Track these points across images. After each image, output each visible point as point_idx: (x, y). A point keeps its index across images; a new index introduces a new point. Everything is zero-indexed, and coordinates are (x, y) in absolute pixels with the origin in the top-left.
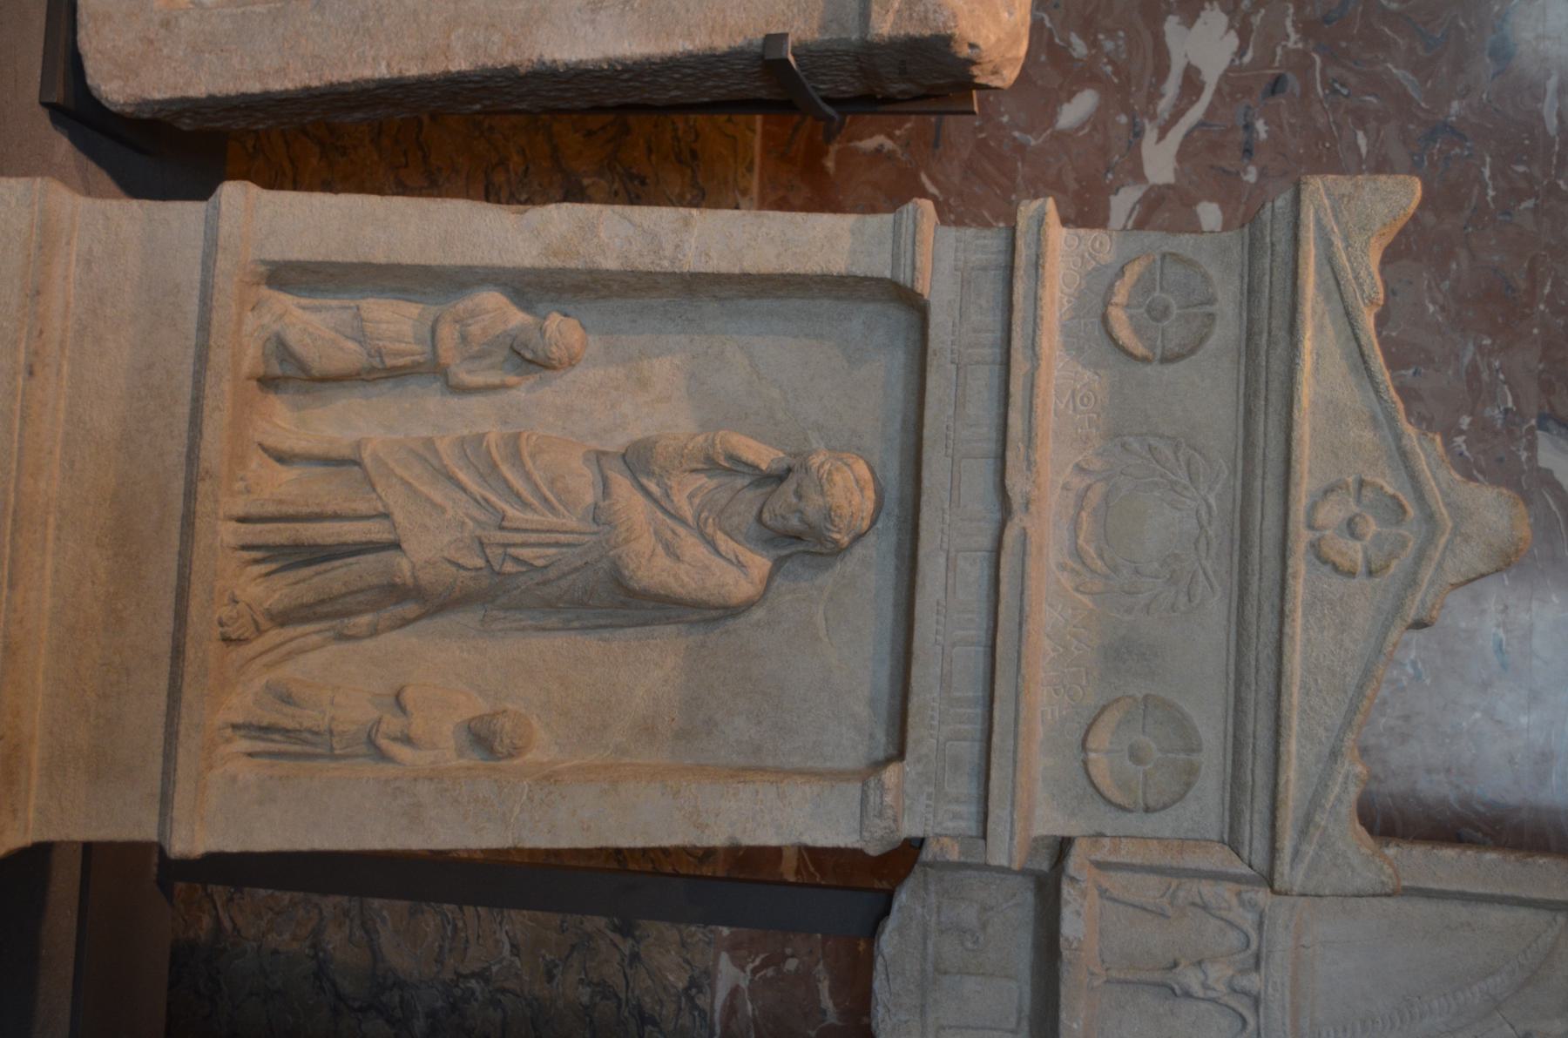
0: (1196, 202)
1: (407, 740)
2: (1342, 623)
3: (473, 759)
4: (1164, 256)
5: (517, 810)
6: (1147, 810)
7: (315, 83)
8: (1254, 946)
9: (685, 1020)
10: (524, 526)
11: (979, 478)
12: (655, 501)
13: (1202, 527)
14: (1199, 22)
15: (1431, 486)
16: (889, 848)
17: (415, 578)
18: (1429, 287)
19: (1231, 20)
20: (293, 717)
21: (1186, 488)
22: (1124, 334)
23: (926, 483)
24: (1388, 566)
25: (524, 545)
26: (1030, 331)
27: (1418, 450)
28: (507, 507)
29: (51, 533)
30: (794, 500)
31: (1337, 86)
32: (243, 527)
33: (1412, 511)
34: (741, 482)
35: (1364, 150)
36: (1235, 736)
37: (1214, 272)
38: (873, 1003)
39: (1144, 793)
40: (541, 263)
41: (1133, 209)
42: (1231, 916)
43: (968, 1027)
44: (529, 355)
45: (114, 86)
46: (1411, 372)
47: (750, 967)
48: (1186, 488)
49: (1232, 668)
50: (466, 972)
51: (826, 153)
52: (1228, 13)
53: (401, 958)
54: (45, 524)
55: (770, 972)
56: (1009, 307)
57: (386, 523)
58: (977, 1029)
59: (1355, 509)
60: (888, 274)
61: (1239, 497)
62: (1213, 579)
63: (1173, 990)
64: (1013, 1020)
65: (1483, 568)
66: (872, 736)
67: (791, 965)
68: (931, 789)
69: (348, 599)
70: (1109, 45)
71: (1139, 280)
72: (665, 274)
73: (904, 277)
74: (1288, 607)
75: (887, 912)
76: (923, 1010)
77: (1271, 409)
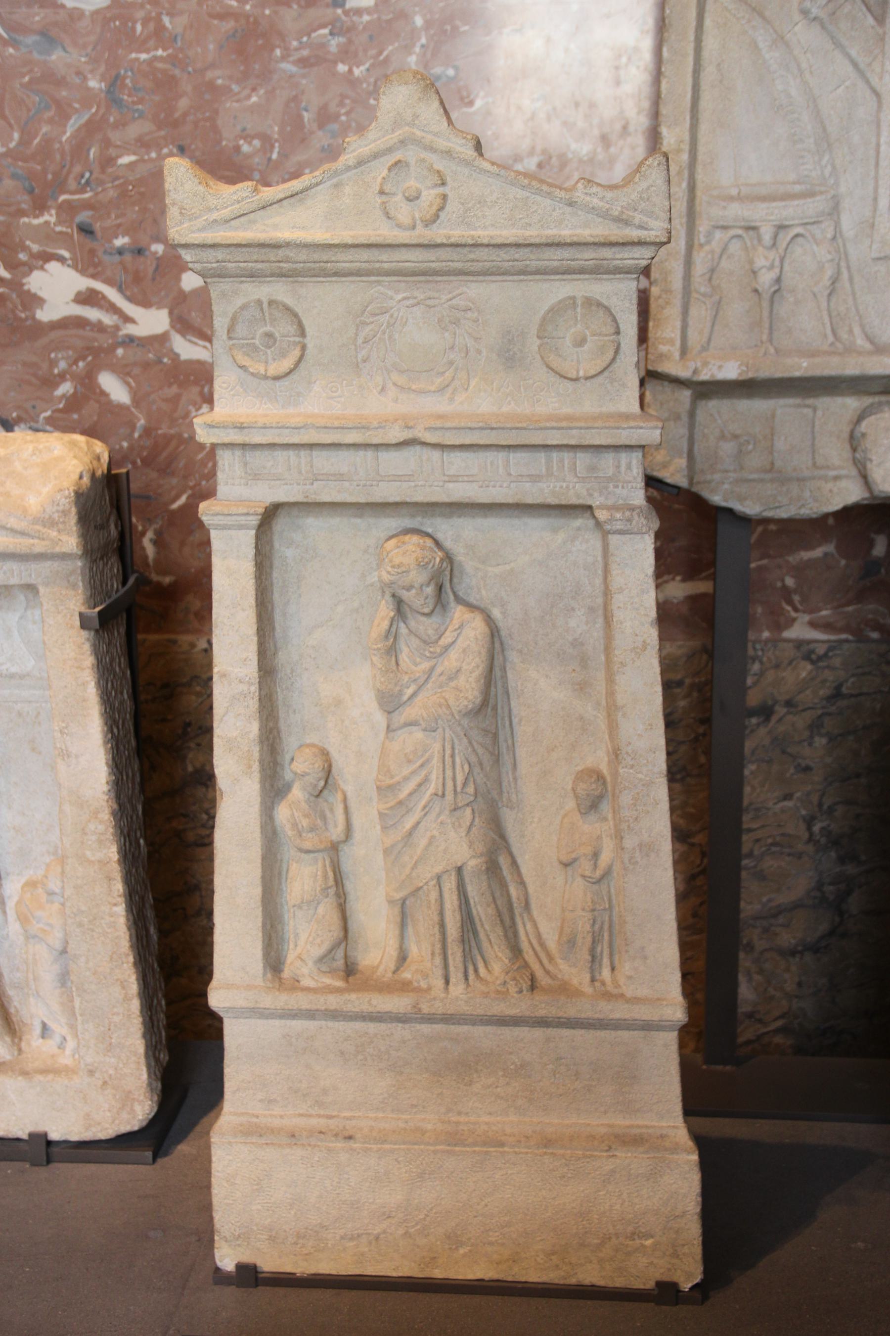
0: (181, 292)
1: (596, 855)
2: (480, 202)
3: (605, 807)
4: (230, 338)
5: (640, 776)
6: (618, 333)
7: (131, 959)
8: (740, 232)
9: (837, 662)
10: (441, 780)
11: (391, 460)
12: (420, 688)
13: (418, 304)
14: (40, 294)
15: (380, 145)
16: (654, 513)
17: (481, 855)
18: (238, 101)
19: (37, 268)
20: (584, 938)
21: (392, 316)
22: (287, 364)
23: (398, 499)
24: (438, 172)
25: (454, 779)
26: (287, 431)
27: (355, 154)
28: (429, 793)
29: (462, 1119)
30: (414, 591)
31: (83, 181)
32: (453, 980)
33: (398, 156)
34: (403, 630)
35: (133, 158)
36: (563, 273)
37: (239, 302)
38: (798, 517)
39: (606, 335)
40: (256, 776)
41: (190, 341)
42: (718, 251)
43: (813, 445)
44: (322, 783)
45: (139, 1111)
46: (305, 114)
47: (793, 614)
48: (392, 316)
49: (515, 278)
50: (806, 835)
51: (159, 584)
52: (31, 270)
53: (800, 884)
54: (457, 1123)
55: (796, 598)
56: (272, 446)
57: (445, 877)
58: (814, 439)
59: (399, 197)
60: (253, 532)
61: (396, 278)
62: (454, 294)
63: (775, 292)
64: (806, 410)
65: (436, 104)
66: (579, 529)
67: (790, 582)
68: (611, 485)
69: (499, 902)
70: (63, 365)
71: (248, 355)
72: (260, 689)
73: (254, 521)
74: (470, 242)
75: (730, 511)
76: (801, 480)
77: (333, 259)
